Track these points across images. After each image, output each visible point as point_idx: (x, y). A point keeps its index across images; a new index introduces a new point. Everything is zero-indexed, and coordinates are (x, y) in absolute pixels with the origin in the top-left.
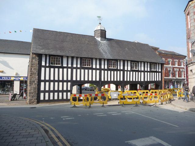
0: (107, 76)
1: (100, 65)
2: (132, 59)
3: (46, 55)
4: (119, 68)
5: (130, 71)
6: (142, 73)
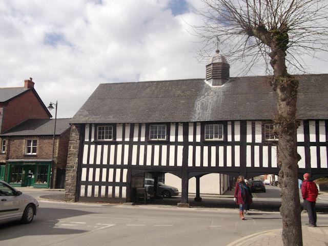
0: (199, 157)
1: (186, 135)
3: (91, 125)
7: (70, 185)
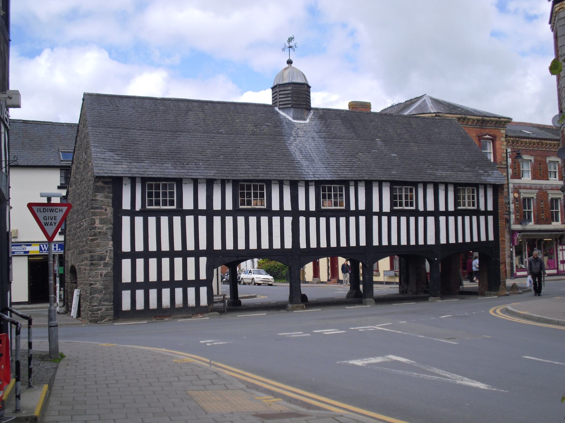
2: (395, 175)
4: (353, 208)
5: (389, 215)
6: (431, 220)
7: (101, 292)
